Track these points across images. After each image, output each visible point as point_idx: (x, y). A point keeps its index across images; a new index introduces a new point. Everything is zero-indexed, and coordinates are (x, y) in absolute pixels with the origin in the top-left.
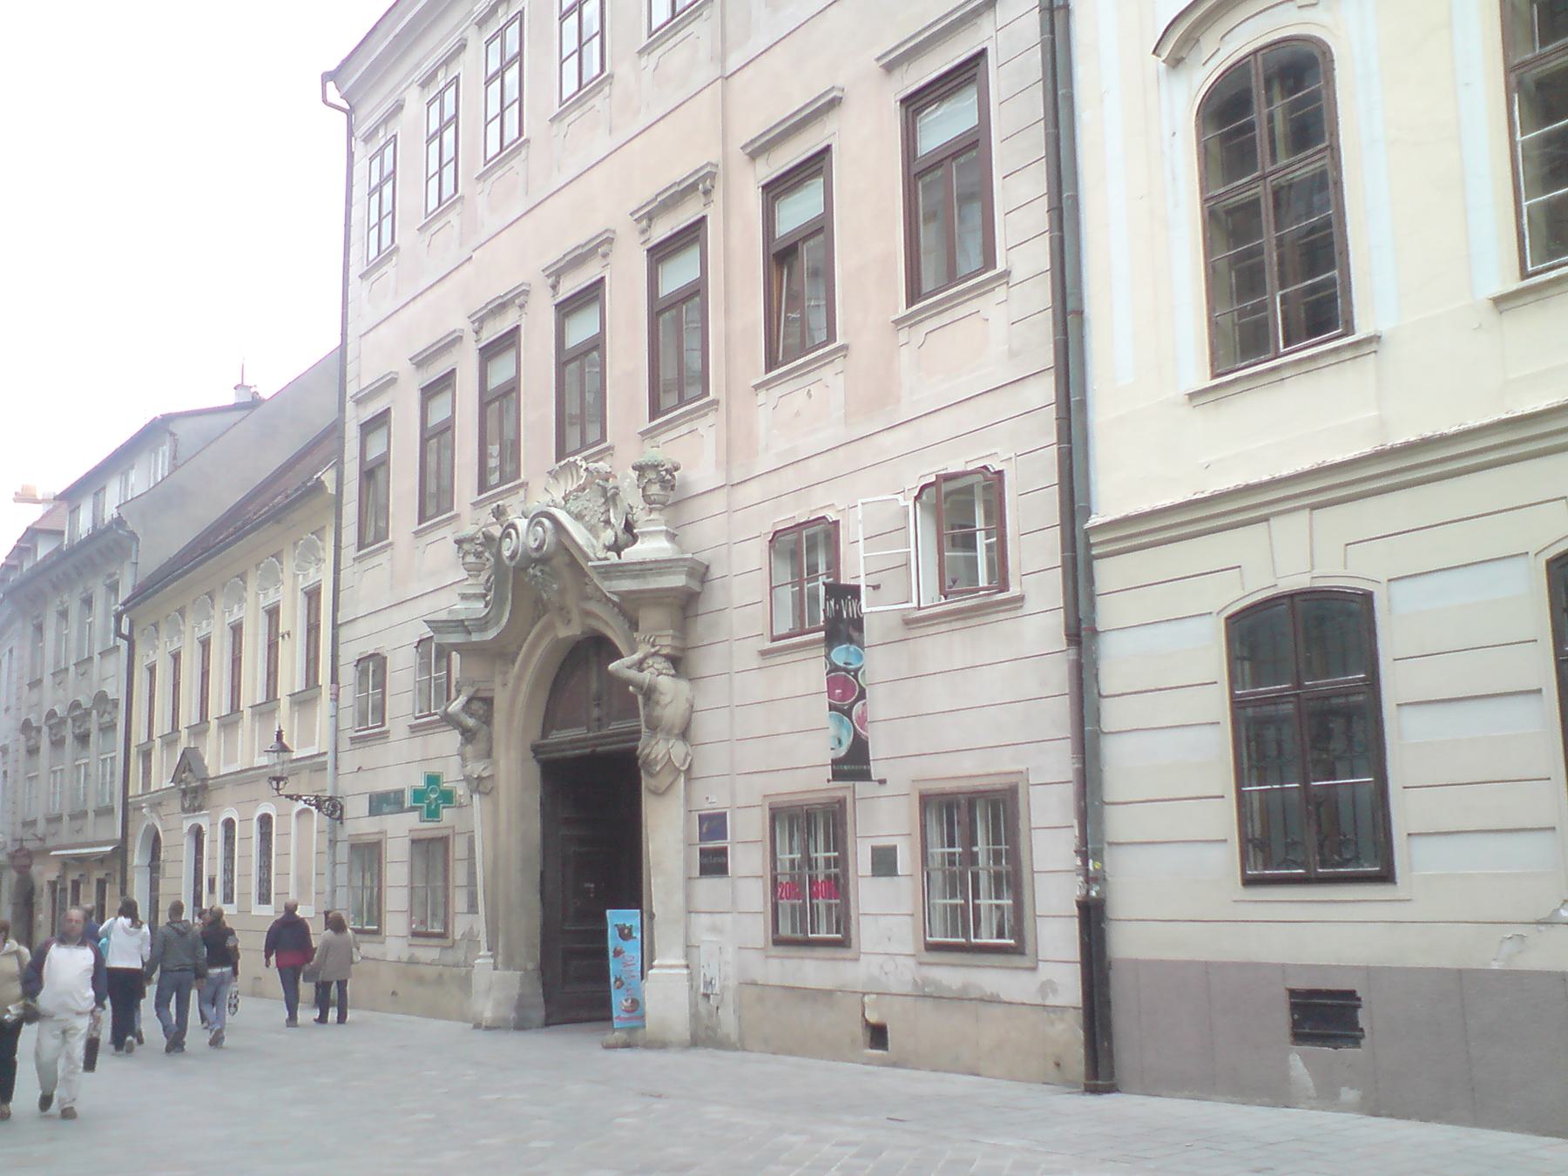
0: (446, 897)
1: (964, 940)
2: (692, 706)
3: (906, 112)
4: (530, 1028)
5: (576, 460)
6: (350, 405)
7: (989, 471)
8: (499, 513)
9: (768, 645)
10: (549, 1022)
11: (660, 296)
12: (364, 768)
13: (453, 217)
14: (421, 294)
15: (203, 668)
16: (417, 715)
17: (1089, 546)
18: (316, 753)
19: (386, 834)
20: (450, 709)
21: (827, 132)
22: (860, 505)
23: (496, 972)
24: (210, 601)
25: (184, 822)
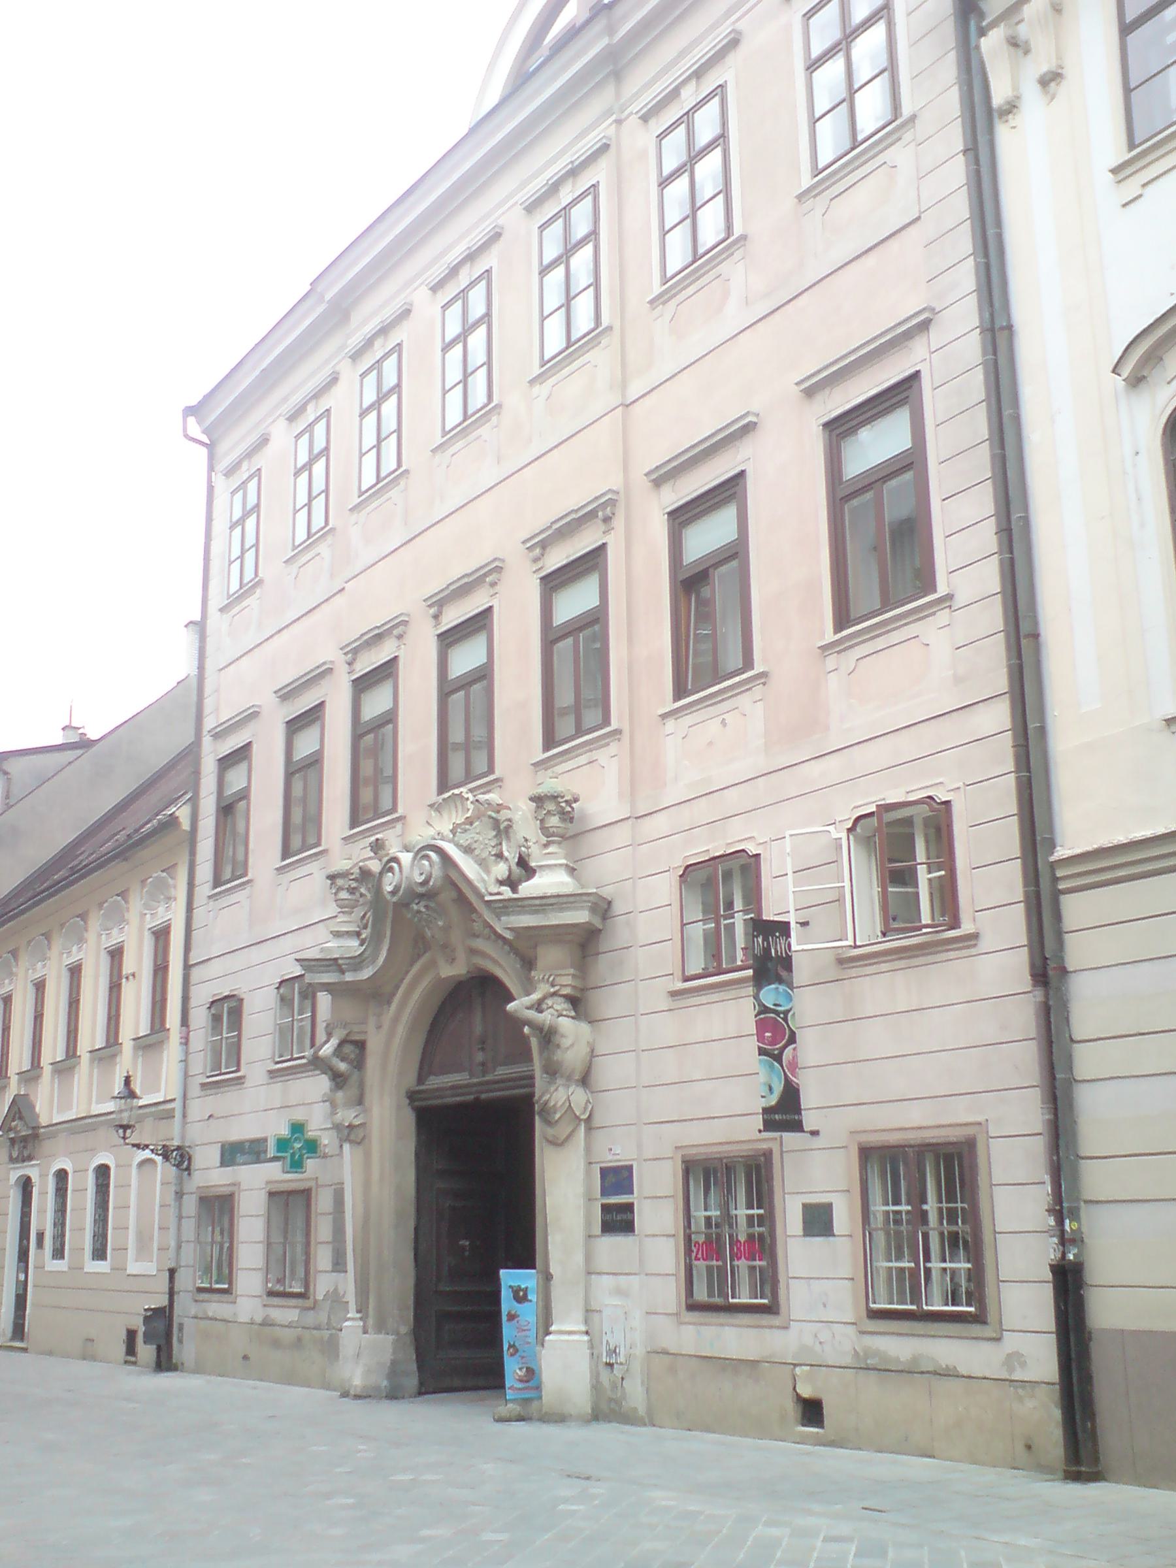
0: (307, 1254)
1: (914, 1307)
2: (592, 1051)
3: (830, 435)
4: (403, 1398)
5: (461, 792)
6: (207, 740)
7: (936, 801)
8: (377, 846)
9: (680, 985)
10: (424, 1390)
11: (554, 625)
12: (215, 1115)
13: (323, 548)
14: (287, 626)
15: (36, 1011)
16: (208, 1074)
17: (1055, 880)
18: (162, 1100)
19: (239, 1188)
20: (321, 1053)
21: (740, 458)
22: (787, 837)
23: (367, 1335)
24: (46, 942)
25: (12, 1172)
